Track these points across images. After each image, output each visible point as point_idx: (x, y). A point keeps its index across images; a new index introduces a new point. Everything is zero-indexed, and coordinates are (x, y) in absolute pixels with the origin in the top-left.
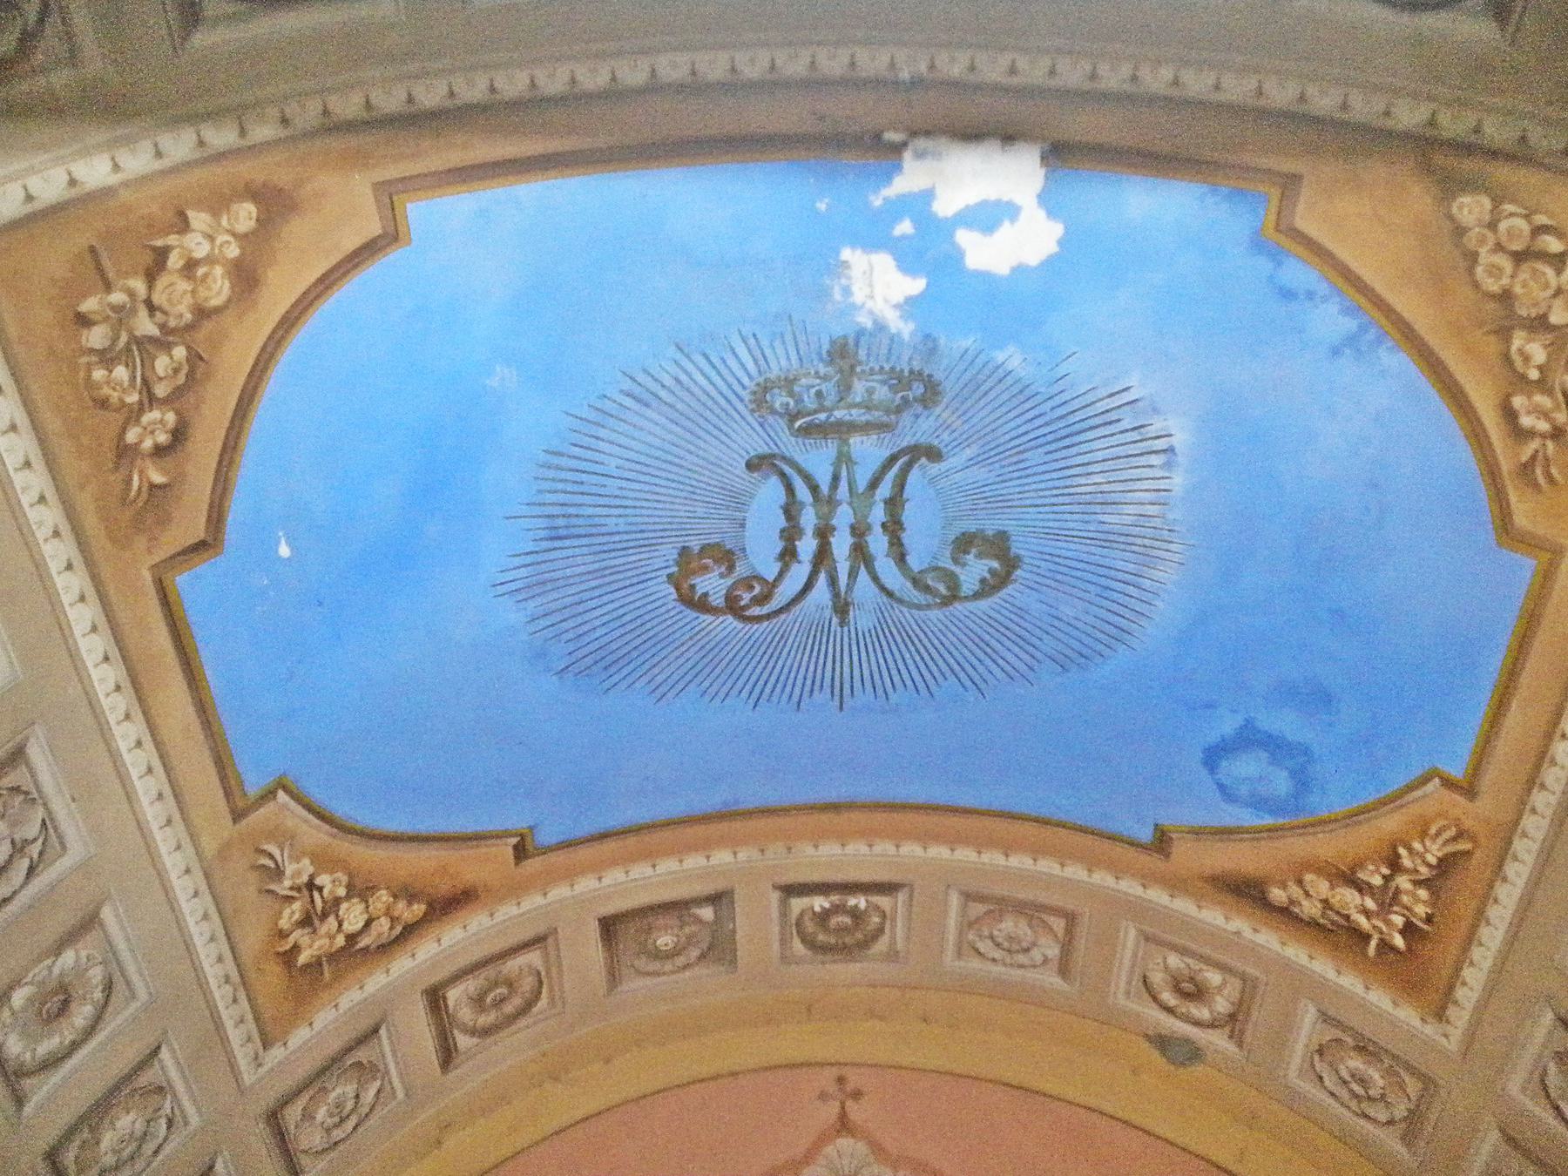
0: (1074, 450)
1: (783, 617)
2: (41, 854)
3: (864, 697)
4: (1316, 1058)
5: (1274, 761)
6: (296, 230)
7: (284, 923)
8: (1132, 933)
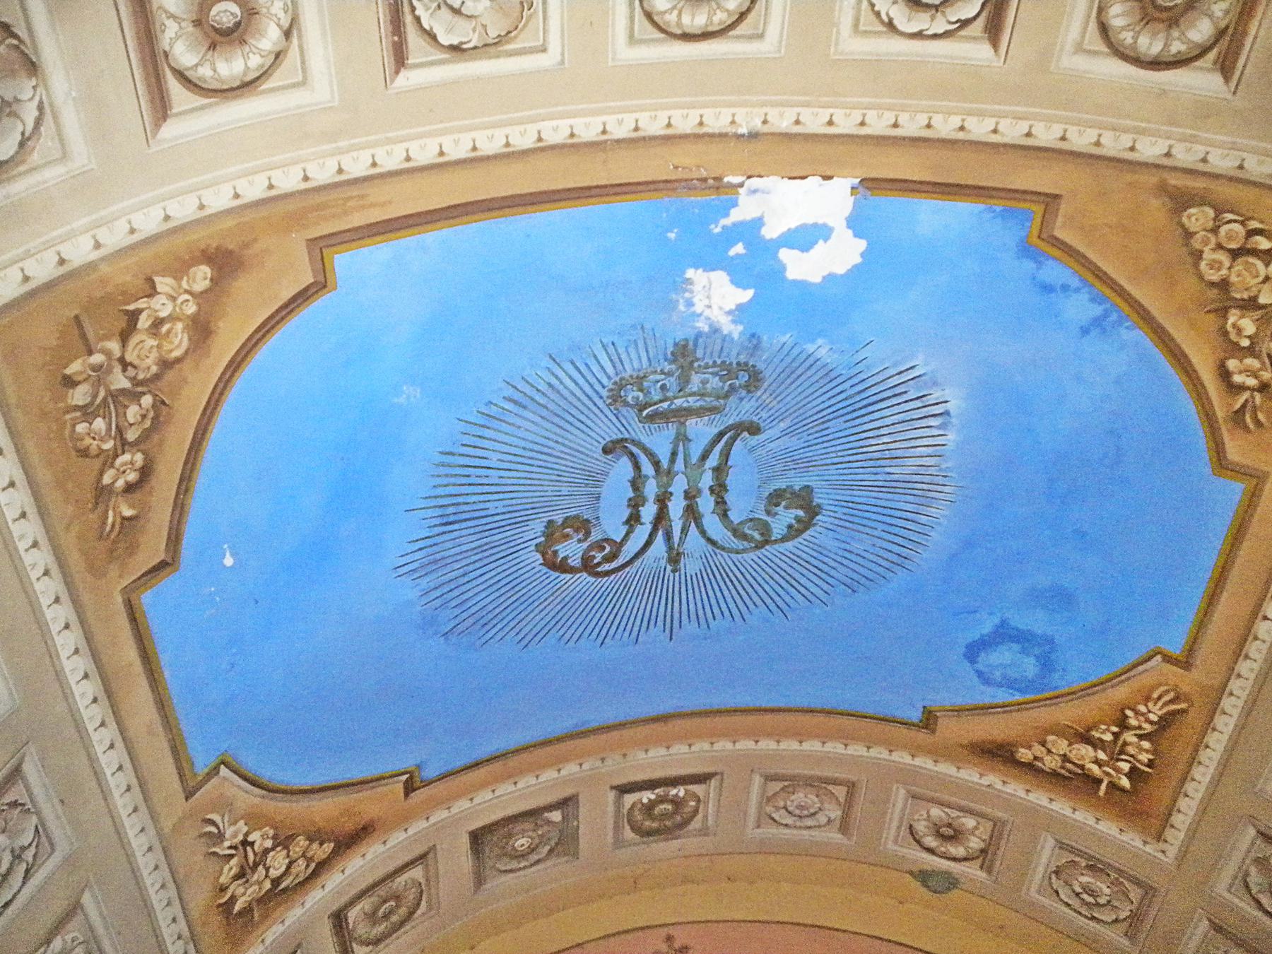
0: (866, 419)
1: (627, 570)
2: (35, 856)
3: (690, 628)
4: (1053, 876)
5: (1024, 651)
6: (243, 286)
7: (223, 880)
8: (902, 792)
